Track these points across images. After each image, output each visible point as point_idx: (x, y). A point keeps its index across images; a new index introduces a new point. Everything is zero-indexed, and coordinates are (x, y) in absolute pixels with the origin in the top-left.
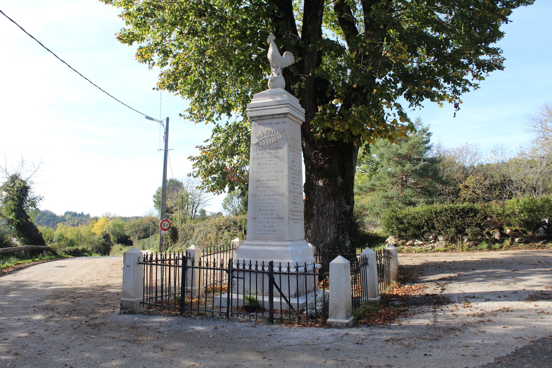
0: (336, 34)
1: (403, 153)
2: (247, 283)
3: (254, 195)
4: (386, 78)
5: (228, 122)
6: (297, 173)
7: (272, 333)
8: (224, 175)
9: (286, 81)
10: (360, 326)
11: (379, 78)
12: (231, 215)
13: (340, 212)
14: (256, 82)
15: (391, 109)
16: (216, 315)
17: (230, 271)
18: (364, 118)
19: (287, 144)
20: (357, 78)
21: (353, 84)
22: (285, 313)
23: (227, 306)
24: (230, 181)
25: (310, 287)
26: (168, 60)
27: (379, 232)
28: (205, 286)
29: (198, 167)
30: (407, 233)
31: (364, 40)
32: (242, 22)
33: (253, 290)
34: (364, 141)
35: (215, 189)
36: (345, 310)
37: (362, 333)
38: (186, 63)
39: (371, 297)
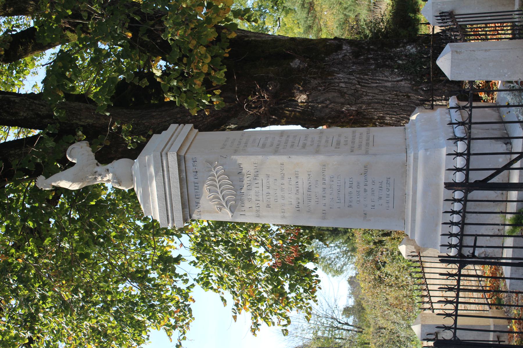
0: (33, 67)
2: (483, 230)
3: (324, 216)
5: (191, 262)
6: (284, 139)
9: (125, 158)
12: (354, 260)
13: (354, 63)
19: (234, 157)
20: (115, 31)
21: (125, 38)
24: (297, 259)
25: (491, 115)
29: (271, 316)
31: (45, 16)
32: (11, 235)
33: (497, 219)
34: (228, 20)
35: (311, 287)
39: (514, 4)
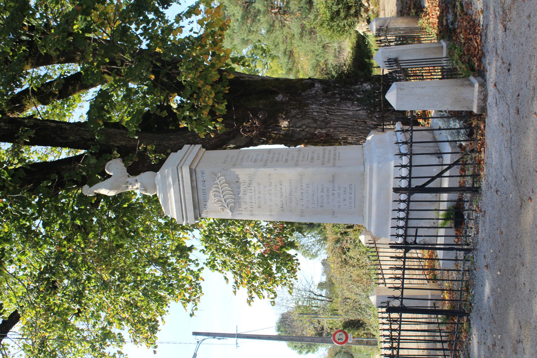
1: (241, 12)
4: (141, 35)
5: (201, 250)
6: (271, 155)
7: (494, 188)
8: (273, 255)
10: (484, 68)
11: (141, 44)
12: (326, 247)
13: (324, 97)
14: (147, 211)
15: (183, 27)
16: (468, 267)
17: (406, 247)
18: (197, 64)
19: (233, 170)
20: (142, 74)
21: (149, 79)
22: (465, 171)
23: (455, 251)
24: (282, 247)
25: (427, 136)
26: (114, 333)
27: (351, 45)
28: (426, 282)
29: (262, 292)
30: (352, 6)
31: (88, 63)
32: (64, 231)
33: (433, 215)
34: (227, 65)
35: (292, 268)
36: (461, 88)
37: (494, 64)
38: (120, 307)
39: (442, 53)
